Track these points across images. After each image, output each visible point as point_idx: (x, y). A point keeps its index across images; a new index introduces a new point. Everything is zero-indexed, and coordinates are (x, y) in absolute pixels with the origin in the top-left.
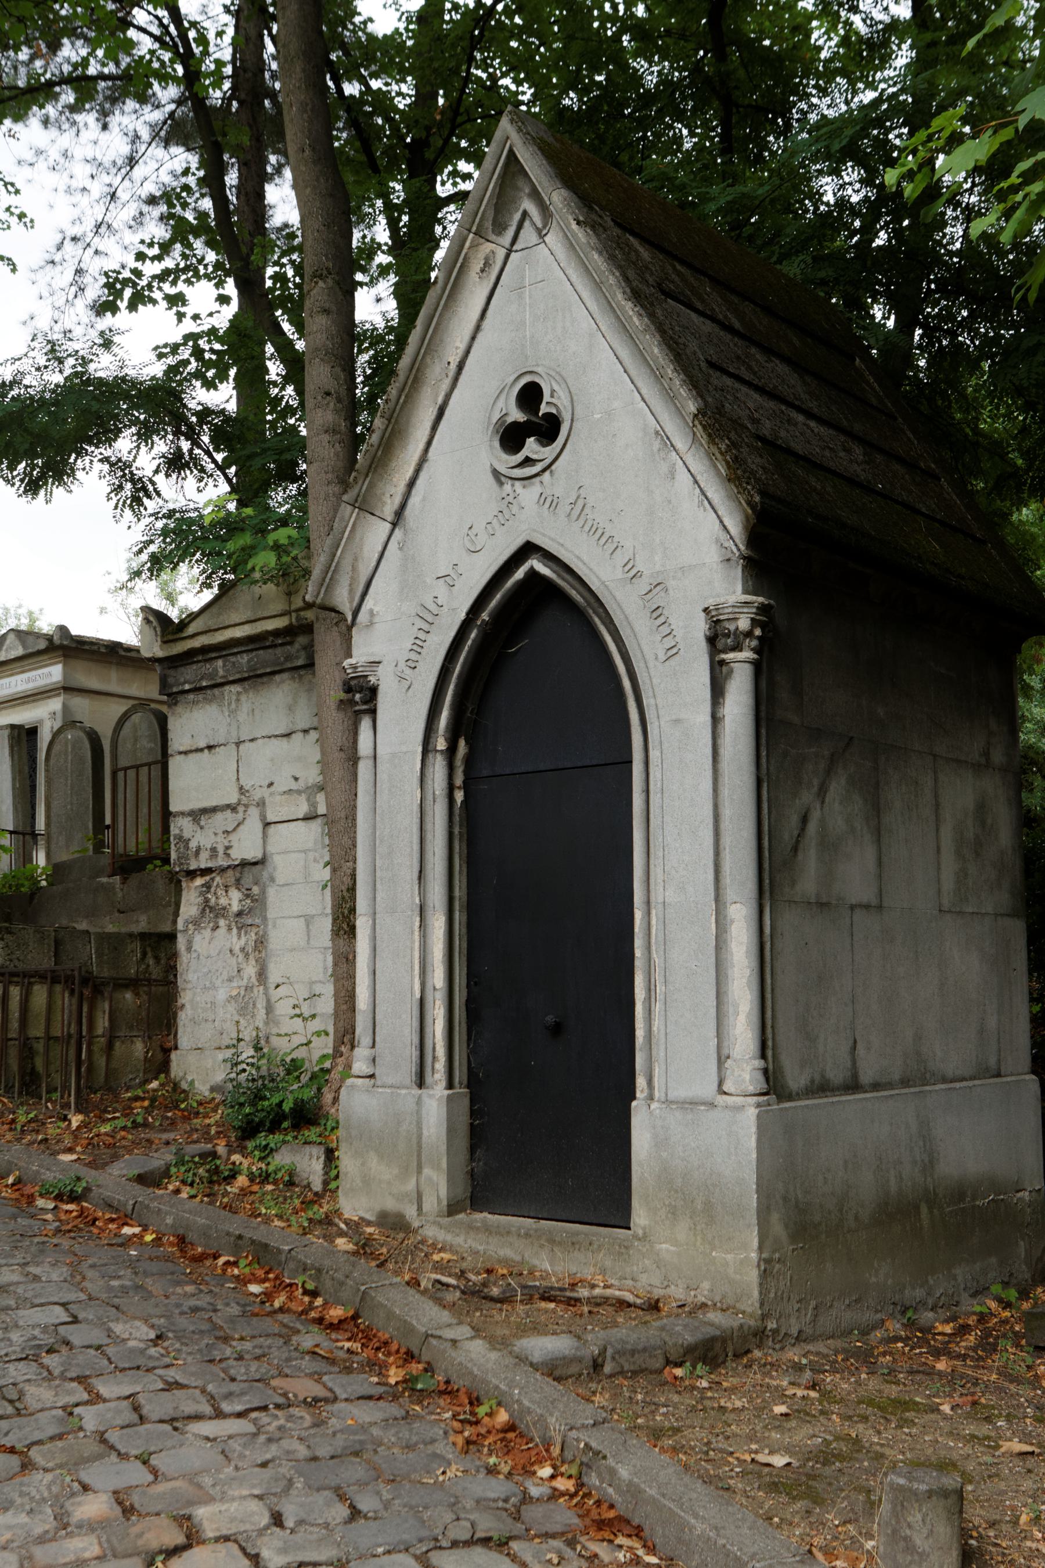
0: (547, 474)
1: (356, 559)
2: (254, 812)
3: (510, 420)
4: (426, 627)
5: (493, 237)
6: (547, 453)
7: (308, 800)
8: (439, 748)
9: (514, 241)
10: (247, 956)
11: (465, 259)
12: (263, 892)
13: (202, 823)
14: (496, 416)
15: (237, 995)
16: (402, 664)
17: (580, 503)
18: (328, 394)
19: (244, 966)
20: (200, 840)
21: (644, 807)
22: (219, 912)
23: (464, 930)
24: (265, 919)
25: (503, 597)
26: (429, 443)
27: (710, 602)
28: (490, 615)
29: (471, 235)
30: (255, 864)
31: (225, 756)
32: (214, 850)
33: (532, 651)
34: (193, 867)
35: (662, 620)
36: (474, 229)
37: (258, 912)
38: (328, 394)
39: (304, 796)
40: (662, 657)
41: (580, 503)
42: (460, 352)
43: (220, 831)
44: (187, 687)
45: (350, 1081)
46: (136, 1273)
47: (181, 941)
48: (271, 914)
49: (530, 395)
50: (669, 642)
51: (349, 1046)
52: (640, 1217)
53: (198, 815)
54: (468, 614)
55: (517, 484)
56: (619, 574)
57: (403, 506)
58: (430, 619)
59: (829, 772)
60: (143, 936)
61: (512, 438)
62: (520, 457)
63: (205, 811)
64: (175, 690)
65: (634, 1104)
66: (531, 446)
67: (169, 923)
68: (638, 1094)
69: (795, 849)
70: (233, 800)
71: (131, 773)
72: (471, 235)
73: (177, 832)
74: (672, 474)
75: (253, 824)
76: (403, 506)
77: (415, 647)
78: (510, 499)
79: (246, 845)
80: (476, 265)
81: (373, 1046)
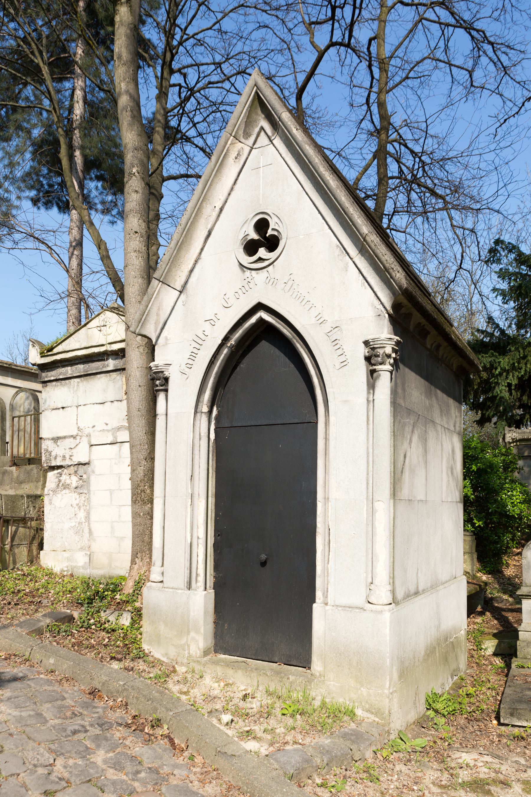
0: (272, 266)
1: (159, 309)
2: (85, 440)
3: (249, 238)
4: (198, 346)
5: (243, 140)
6: (273, 255)
7: (113, 434)
8: (203, 411)
9: (254, 144)
10: (79, 508)
11: (227, 150)
12: (89, 478)
13: (58, 444)
14: (242, 236)
15: (82, 532)
16: (184, 366)
17: (290, 282)
18: (136, 232)
19: (78, 512)
20: (54, 452)
21: (324, 447)
22: (66, 486)
23: (213, 507)
24: (89, 491)
25: (243, 332)
26: (202, 249)
27: (369, 337)
28: (235, 341)
29: (232, 137)
30: (85, 464)
31: (71, 412)
32: (64, 456)
33: (263, 362)
34: (53, 464)
35: (338, 346)
36: (233, 134)
37: (85, 487)
38: (136, 232)
39: (110, 433)
40: (338, 366)
41: (290, 282)
42: (223, 199)
43: (67, 448)
44: (52, 378)
45: (149, 584)
46: (35, 703)
47: (46, 500)
48: (92, 488)
49: (262, 225)
50: (342, 358)
51: (140, 559)
52: (317, 665)
53: (56, 440)
54: (222, 341)
55: (253, 272)
56: (313, 321)
57: (186, 283)
58: (200, 342)
59: (413, 432)
60: (28, 496)
61: (251, 248)
62: (255, 257)
63: (59, 438)
64: (46, 379)
65: (314, 605)
66: (262, 252)
67: (40, 489)
68: (317, 600)
69: (402, 472)
70: (74, 433)
71: (22, 419)
72: (232, 137)
73: (46, 447)
74: (346, 269)
75: (84, 444)
76: (186, 283)
77: (191, 357)
78: (249, 280)
79: (81, 456)
80: (233, 155)
81: (163, 566)
